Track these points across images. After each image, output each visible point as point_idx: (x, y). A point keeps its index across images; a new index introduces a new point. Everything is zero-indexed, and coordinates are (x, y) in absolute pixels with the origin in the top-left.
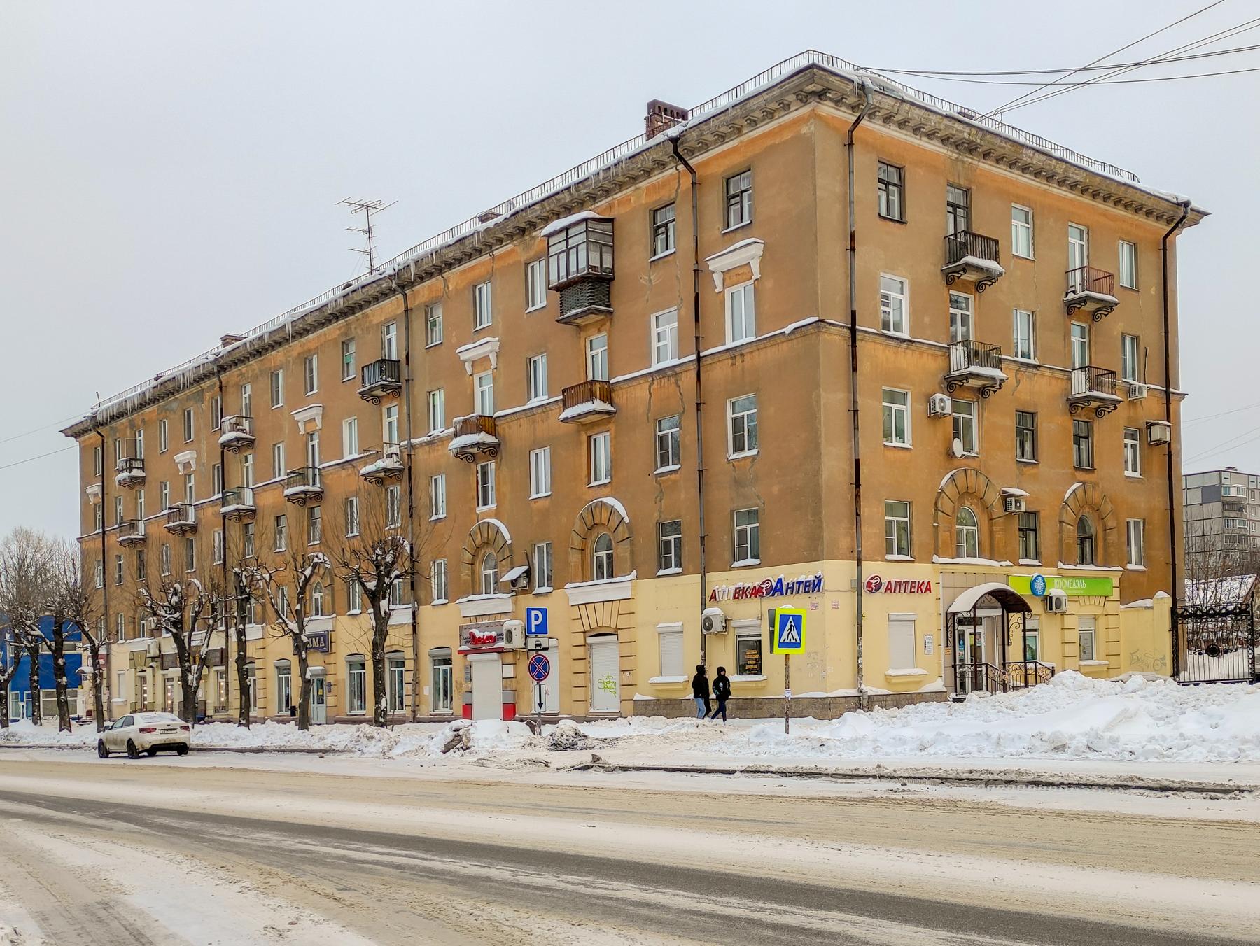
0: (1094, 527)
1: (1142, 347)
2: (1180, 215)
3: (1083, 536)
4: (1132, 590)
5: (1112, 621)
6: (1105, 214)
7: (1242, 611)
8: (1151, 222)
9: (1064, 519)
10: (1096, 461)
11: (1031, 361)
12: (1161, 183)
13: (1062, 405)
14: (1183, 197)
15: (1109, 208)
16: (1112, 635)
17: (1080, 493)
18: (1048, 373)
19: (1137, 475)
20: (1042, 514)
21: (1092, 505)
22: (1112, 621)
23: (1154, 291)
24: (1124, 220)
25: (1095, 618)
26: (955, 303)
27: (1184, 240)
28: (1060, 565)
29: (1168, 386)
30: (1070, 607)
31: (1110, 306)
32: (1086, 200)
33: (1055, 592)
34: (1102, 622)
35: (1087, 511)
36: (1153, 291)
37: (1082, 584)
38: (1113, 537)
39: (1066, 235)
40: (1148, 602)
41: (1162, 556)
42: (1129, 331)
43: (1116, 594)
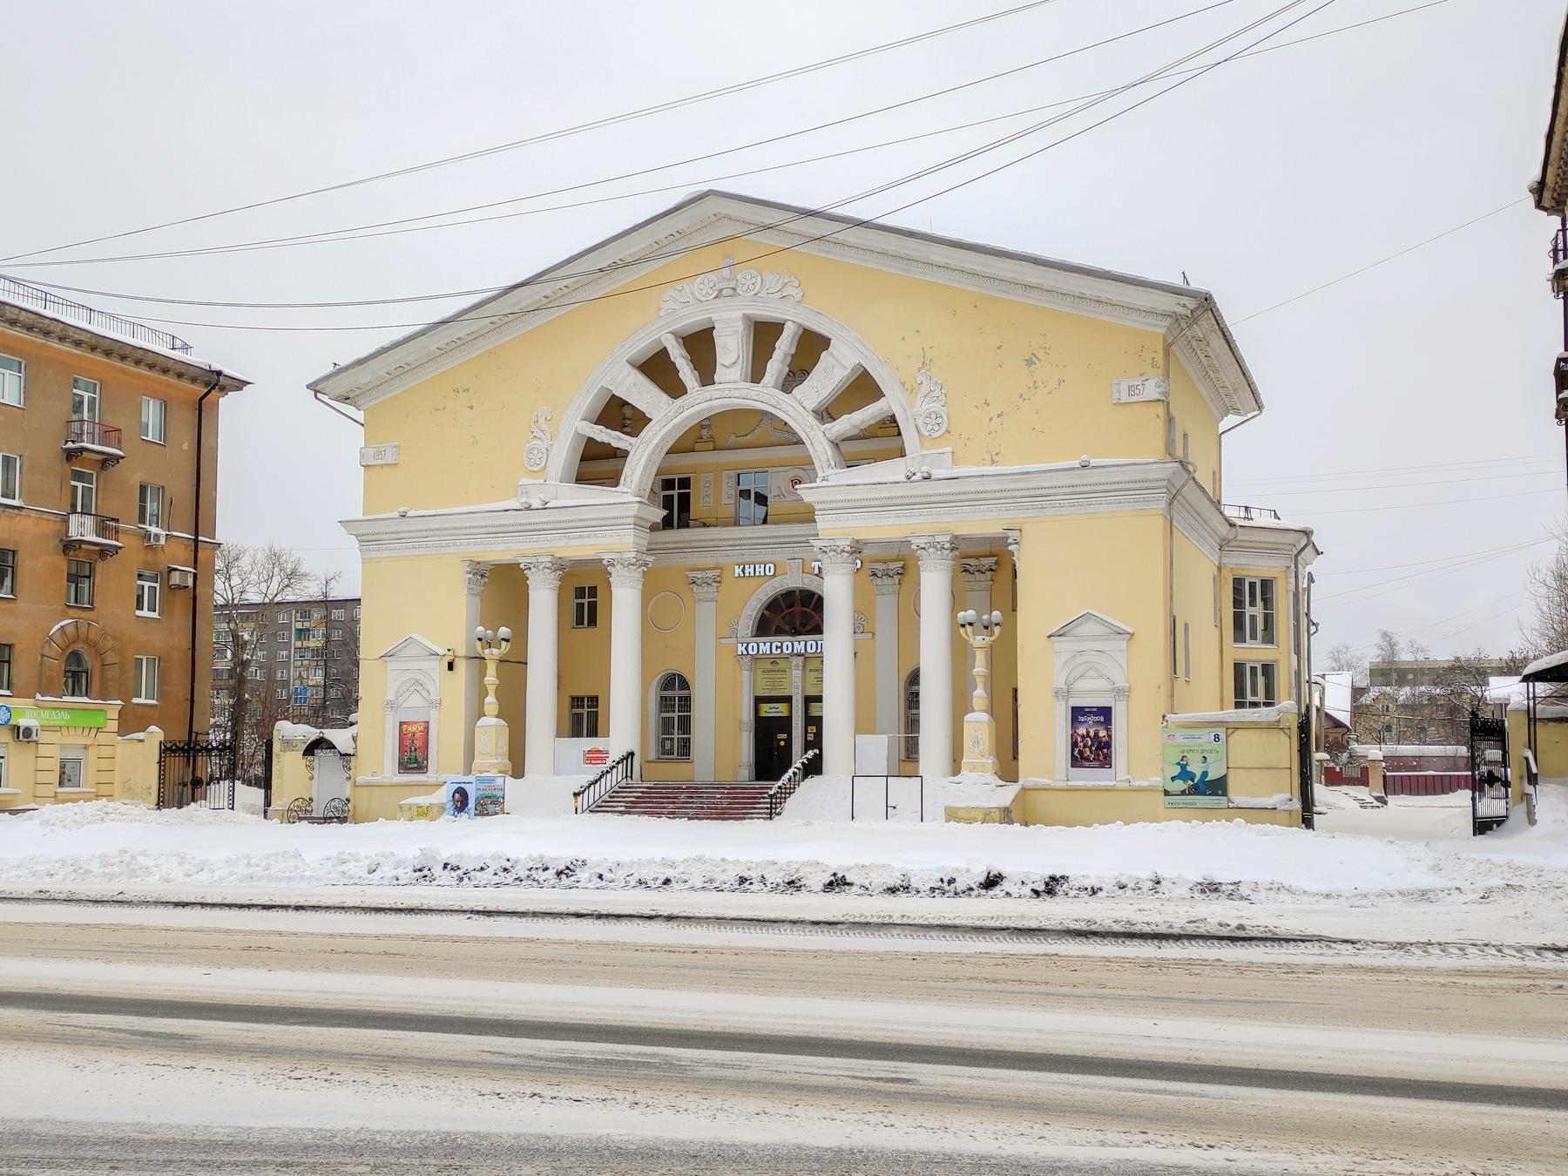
0: (89, 661)
1: (167, 498)
2: (216, 382)
3: (74, 668)
4: (131, 722)
5: (106, 752)
6: (124, 372)
7: (225, 748)
8: (185, 384)
9: (46, 652)
10: (96, 599)
11: (16, 503)
12: (199, 357)
13: (54, 544)
14: (216, 367)
15: (129, 366)
16: (104, 764)
17: (71, 630)
18: (34, 514)
19: (155, 615)
20: (17, 647)
21: (87, 641)
22: (106, 752)
23: (187, 446)
24: (149, 379)
25: (86, 747)
26: (79, 476)
27: (228, 405)
28: (38, 696)
29: (197, 535)
30: (43, 737)
31: (118, 458)
32: (98, 357)
33: (23, 722)
34: (92, 752)
35: (80, 647)
36: (185, 446)
37: (66, 715)
38: (113, 672)
39: (138, 410)
40: (141, 735)
41: (180, 690)
42: (154, 480)
43: (114, 726)
